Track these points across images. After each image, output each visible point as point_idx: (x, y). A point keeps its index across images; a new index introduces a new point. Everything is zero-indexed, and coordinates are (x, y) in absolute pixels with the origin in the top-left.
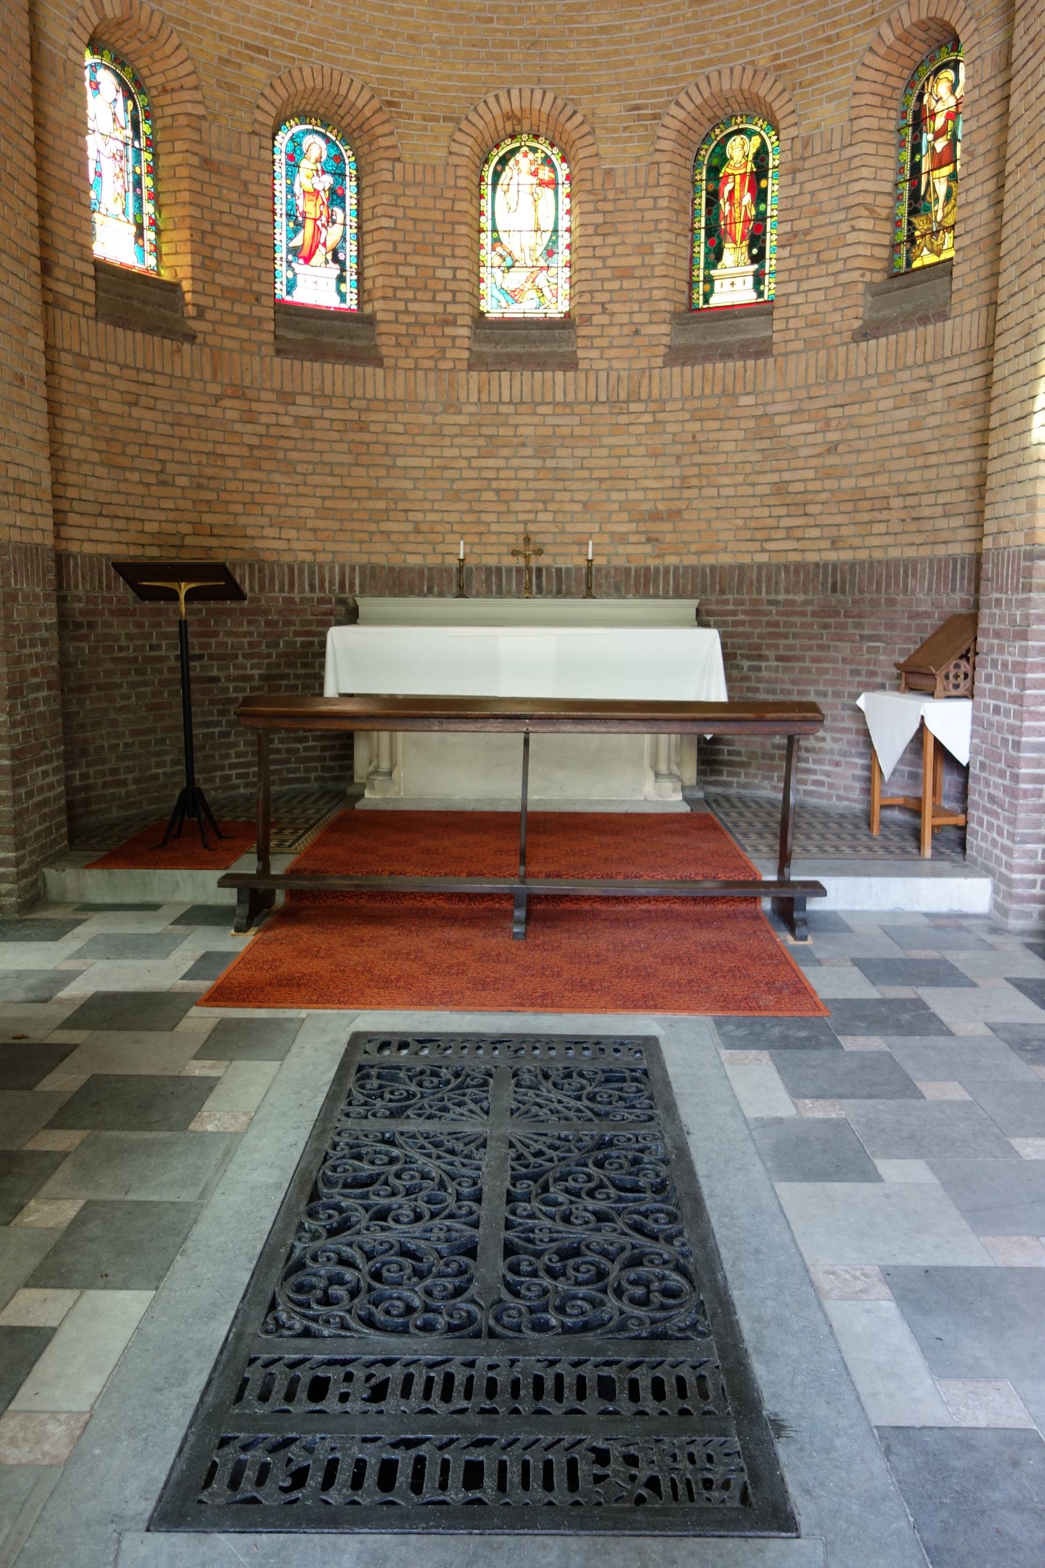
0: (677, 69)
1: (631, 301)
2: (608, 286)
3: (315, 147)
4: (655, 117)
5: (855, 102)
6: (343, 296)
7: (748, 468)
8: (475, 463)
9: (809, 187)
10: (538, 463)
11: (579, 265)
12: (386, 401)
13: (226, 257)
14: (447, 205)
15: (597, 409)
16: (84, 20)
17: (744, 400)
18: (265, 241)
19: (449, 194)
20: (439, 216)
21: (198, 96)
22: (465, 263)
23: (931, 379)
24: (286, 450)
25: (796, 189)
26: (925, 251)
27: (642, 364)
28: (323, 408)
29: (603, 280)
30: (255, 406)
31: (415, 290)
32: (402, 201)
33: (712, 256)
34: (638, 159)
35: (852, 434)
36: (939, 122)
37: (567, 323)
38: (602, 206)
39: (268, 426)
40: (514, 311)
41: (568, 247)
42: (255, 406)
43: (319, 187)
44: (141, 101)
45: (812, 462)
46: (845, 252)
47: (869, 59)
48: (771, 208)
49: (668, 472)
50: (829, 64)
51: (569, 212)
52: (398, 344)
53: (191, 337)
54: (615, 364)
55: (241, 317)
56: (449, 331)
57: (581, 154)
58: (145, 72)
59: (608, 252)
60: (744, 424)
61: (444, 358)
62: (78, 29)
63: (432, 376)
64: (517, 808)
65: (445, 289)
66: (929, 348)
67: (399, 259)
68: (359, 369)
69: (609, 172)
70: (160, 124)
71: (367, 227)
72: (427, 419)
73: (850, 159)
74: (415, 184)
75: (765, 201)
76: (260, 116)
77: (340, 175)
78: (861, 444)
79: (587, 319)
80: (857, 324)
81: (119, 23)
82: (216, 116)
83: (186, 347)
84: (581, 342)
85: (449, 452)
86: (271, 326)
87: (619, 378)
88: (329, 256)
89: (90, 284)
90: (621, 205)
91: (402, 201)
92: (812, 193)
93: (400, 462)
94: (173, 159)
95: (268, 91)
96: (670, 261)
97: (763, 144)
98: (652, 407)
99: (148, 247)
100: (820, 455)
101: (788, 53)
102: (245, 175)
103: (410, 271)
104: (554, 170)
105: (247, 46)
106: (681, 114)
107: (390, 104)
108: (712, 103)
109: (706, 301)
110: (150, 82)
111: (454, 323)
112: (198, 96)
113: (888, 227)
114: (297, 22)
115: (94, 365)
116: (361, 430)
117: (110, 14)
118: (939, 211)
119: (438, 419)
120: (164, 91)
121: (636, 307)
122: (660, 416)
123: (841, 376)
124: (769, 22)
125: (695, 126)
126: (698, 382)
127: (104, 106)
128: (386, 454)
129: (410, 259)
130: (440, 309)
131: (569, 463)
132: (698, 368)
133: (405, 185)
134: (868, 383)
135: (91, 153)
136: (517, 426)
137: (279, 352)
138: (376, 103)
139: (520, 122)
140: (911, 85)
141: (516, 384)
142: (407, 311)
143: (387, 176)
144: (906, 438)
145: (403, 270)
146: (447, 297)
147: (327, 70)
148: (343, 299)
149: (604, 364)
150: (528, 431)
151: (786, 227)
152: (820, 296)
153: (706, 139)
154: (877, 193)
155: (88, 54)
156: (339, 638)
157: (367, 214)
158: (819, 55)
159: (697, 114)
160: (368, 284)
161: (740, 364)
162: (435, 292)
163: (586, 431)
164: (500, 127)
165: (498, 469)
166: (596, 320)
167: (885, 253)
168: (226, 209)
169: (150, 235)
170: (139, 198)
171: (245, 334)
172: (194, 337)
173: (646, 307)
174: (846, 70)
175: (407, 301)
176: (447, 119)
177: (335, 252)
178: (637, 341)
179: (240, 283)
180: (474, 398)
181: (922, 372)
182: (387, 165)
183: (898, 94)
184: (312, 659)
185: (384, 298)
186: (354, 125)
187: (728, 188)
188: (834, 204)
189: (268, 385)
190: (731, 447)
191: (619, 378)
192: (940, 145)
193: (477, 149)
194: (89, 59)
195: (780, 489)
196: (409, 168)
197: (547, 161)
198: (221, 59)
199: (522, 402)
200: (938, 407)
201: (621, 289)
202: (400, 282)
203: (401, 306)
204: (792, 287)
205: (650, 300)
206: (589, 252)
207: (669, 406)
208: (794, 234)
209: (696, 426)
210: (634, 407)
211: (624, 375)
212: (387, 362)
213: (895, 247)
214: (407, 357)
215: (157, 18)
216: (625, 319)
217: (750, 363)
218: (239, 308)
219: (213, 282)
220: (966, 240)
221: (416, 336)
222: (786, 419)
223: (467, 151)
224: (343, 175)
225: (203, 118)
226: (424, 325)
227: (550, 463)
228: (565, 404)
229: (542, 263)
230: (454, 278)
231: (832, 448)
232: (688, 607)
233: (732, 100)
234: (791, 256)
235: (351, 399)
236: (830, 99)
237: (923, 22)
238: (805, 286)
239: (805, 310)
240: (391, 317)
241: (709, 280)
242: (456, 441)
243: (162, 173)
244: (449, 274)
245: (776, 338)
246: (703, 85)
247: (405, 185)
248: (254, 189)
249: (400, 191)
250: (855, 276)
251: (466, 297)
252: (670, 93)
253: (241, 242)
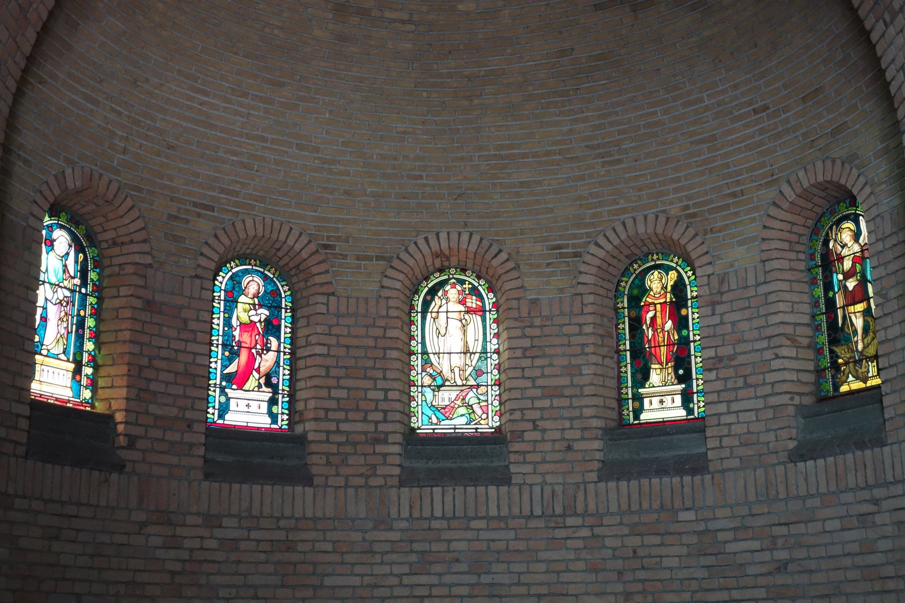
0: (594, 215)
1: (562, 418)
2: (538, 404)
3: (254, 284)
4: (576, 255)
5: (765, 246)
6: (274, 417)
7: (694, 585)
8: (406, 580)
9: (729, 318)
10: (473, 579)
11: (508, 385)
12: (315, 519)
13: (162, 388)
14: (379, 332)
15: (533, 524)
16: (47, 193)
17: (684, 516)
18: (201, 372)
19: (382, 323)
20: (371, 343)
21: (146, 247)
22: (396, 385)
23: (876, 502)
24: (209, 574)
25: (716, 320)
26: (851, 378)
27: (578, 479)
28: (249, 530)
29: (533, 399)
30: (180, 531)
31: (347, 411)
32: (335, 330)
33: (639, 376)
34: (561, 290)
35: (800, 554)
36: (847, 264)
37: (497, 438)
38: (529, 331)
39: (192, 550)
40: (446, 427)
41: (495, 321)
42: (180, 531)
43: (256, 319)
44: (91, 252)
45: (762, 581)
46: (770, 377)
47: (773, 211)
48: (694, 334)
49: (609, 588)
50: (736, 214)
51: (497, 336)
52: (328, 463)
53: (120, 467)
54: (549, 479)
55: (172, 443)
56: (379, 448)
57: (507, 286)
58: (98, 229)
59: (537, 372)
60: (686, 539)
61: (375, 475)
62: (39, 199)
63: (362, 493)
65: (376, 410)
66: (870, 472)
67: (332, 382)
68: (288, 489)
69: (534, 302)
70: (107, 272)
71: (300, 353)
72: (357, 536)
73: (766, 295)
74: (348, 315)
75: (687, 327)
76: (203, 262)
77: (275, 308)
78: (812, 565)
79: (519, 435)
80: (792, 445)
81: (78, 192)
82: (161, 264)
83: (114, 477)
84: (513, 458)
85: (377, 570)
86: (201, 451)
87: (553, 492)
88: (262, 381)
89: (24, 424)
90: (547, 331)
91: (335, 330)
92: (733, 323)
93: (328, 581)
94: (117, 303)
95: (212, 240)
96: (598, 381)
97: (680, 276)
98: (590, 521)
99: (84, 381)
100: (769, 574)
101: (696, 205)
102: (185, 314)
103: (343, 394)
104: (480, 298)
105: (195, 205)
106: (601, 253)
107: (326, 247)
108: (629, 243)
109: (636, 417)
110: (100, 237)
111: (385, 442)
112: (146, 247)
113: (811, 354)
114: (241, 183)
115: (18, 502)
116: (288, 550)
117: (70, 185)
119: (368, 536)
120: (115, 244)
121: (567, 424)
122: (597, 530)
123: (782, 495)
124: (677, 180)
125: (615, 262)
126: (635, 497)
127: (57, 258)
128: (314, 573)
129: (342, 382)
130: (371, 428)
131: (505, 579)
132: (634, 483)
133: (338, 315)
134: (810, 503)
135: (40, 302)
136: (449, 541)
137: (207, 476)
138: (313, 247)
139: (448, 259)
140: (815, 231)
141: (449, 499)
142: (338, 431)
143: (323, 309)
144: (859, 560)
145: (335, 393)
146: (379, 416)
147: (268, 221)
148: (274, 421)
149: (538, 479)
150: (462, 546)
151: (711, 353)
152: (752, 416)
153: (625, 272)
154: (796, 324)
155: (47, 218)
157: (301, 342)
158: (727, 207)
159: (616, 253)
160: (300, 406)
161: (676, 480)
162: (366, 412)
163: (522, 545)
164: (429, 263)
165: (431, 586)
166: (528, 436)
167: (811, 378)
168: (165, 344)
169: (88, 370)
170: (80, 338)
171: (175, 460)
172: (124, 466)
173: (577, 424)
174: (753, 220)
175: (338, 422)
176: (379, 258)
177: (268, 376)
178: (570, 456)
179: (174, 412)
180: (405, 514)
181: (866, 495)
182: (323, 299)
183: (804, 239)
185: (315, 419)
186: (291, 265)
187: (650, 315)
188: (755, 334)
189: (194, 509)
190: (675, 562)
191: (553, 492)
192: (851, 284)
193: (408, 283)
194: (47, 221)
196: (343, 301)
197: (475, 291)
198: (171, 217)
199: (455, 517)
200: (889, 530)
201: (552, 407)
202: (333, 404)
203: (332, 426)
204: (723, 408)
205: (581, 417)
206: (519, 373)
207: (606, 520)
208: (720, 359)
209: (636, 541)
210: (570, 521)
211: (559, 489)
212: (316, 481)
213: (819, 372)
214: (338, 475)
215: (114, 187)
216: (557, 435)
217: (687, 479)
218: (170, 436)
219: (147, 413)
220: (892, 373)
221: (347, 454)
222: (730, 535)
223: (398, 285)
224: (279, 308)
225: (150, 266)
226: (355, 444)
227: (485, 579)
228: (499, 518)
229: (472, 382)
230: (386, 399)
231: (782, 567)
233: (647, 242)
234: (718, 379)
235: (278, 519)
236: (740, 243)
237: (820, 184)
238: (735, 407)
239: (737, 429)
240: (323, 437)
241: (638, 398)
242: (387, 558)
243: (105, 315)
244: (380, 395)
245: (711, 455)
246: (620, 229)
247: (338, 315)
248: (193, 325)
249: (334, 321)
250: (785, 399)
251: (398, 417)
252: (588, 235)
253: (176, 373)
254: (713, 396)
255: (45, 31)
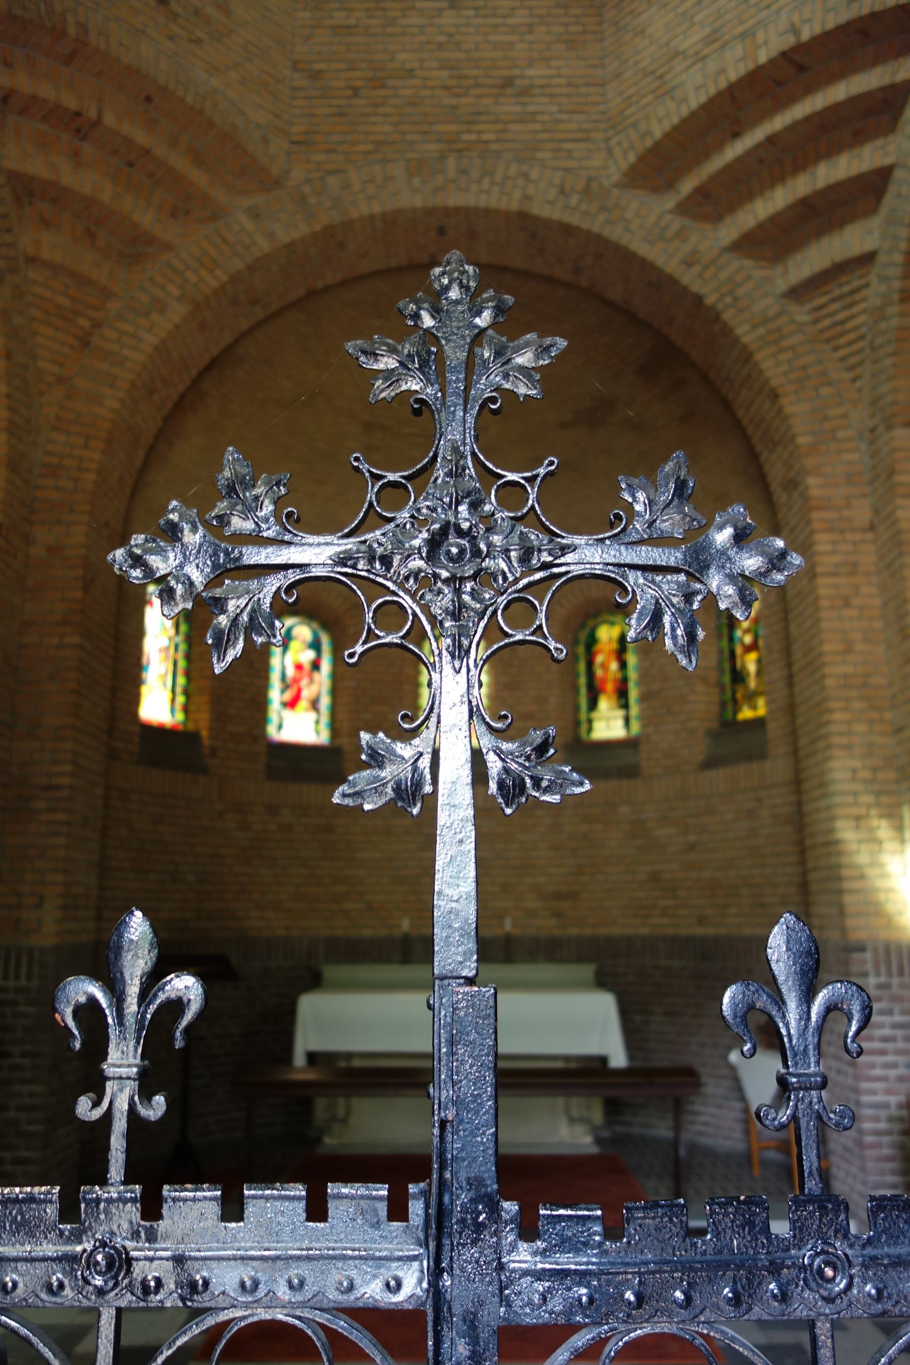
6: (318, 732)
48: (632, 675)
53: (204, 770)
64: (137, 1083)
118: (752, 683)
153: (583, 626)
156: (312, 1008)
184: (284, 1021)
195: (655, 877)
213: (723, 704)
231: (692, 847)
232: (587, 971)
241: (590, 722)
254: (645, 719)
255: (151, 450)
